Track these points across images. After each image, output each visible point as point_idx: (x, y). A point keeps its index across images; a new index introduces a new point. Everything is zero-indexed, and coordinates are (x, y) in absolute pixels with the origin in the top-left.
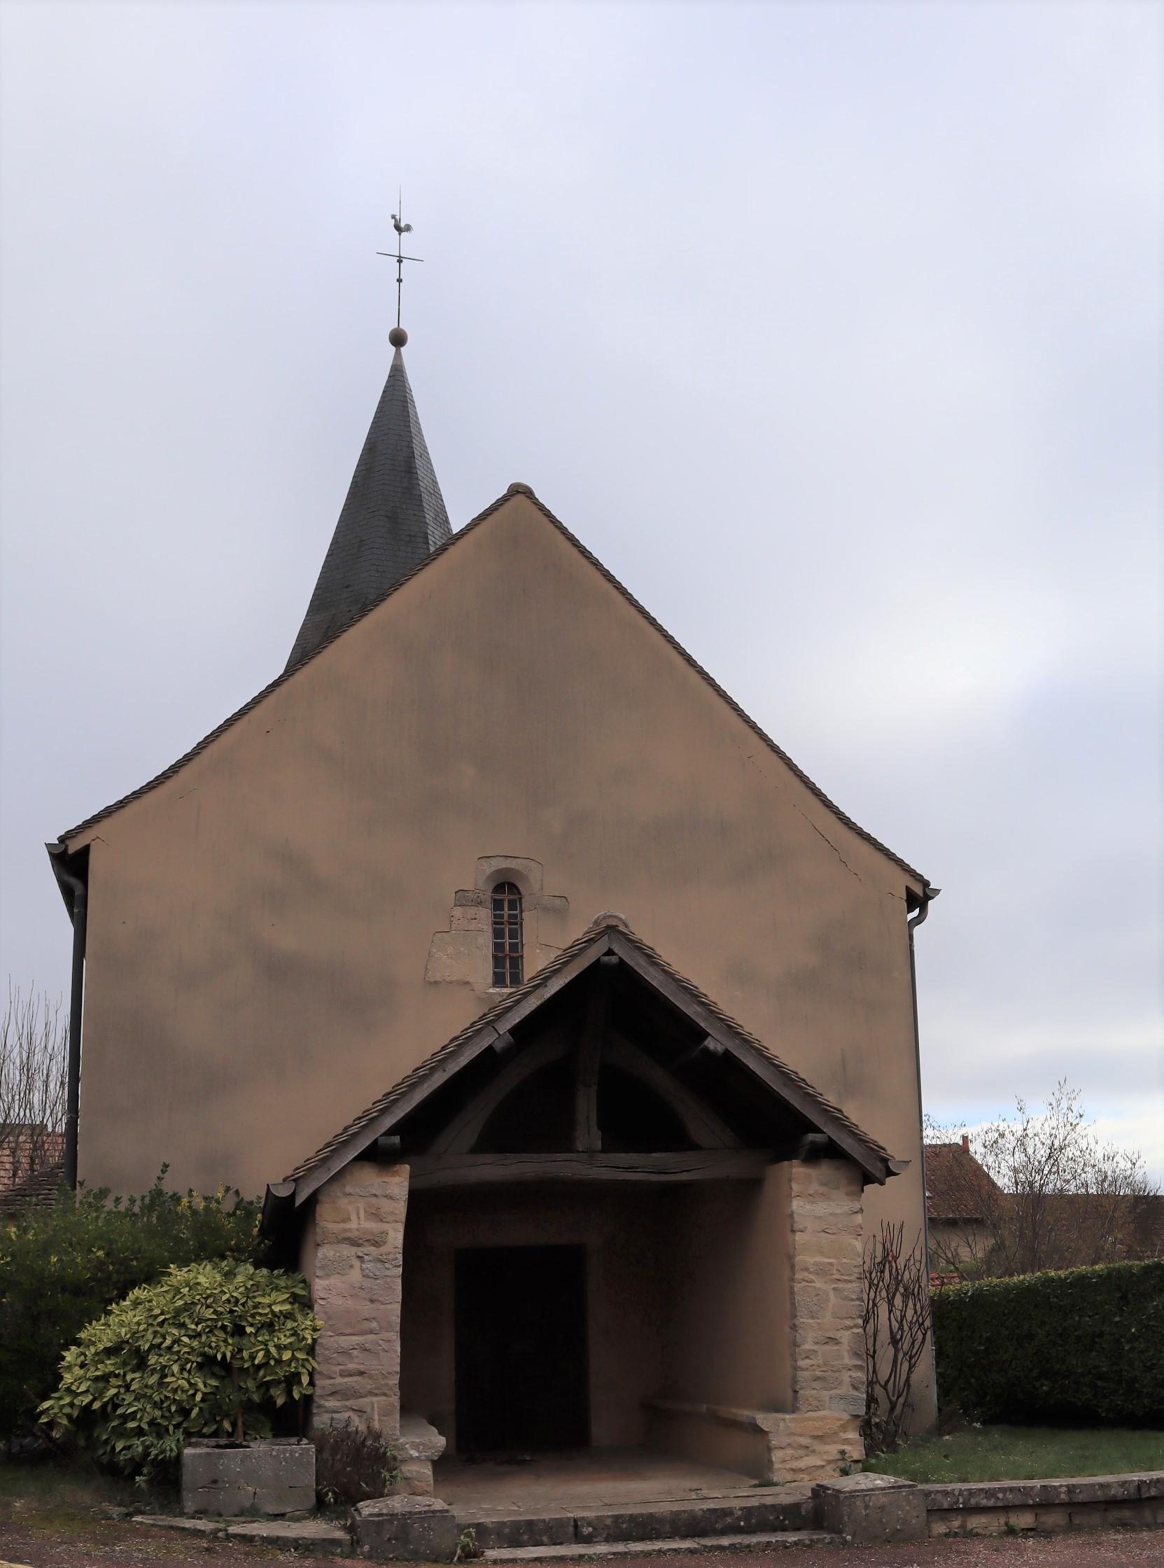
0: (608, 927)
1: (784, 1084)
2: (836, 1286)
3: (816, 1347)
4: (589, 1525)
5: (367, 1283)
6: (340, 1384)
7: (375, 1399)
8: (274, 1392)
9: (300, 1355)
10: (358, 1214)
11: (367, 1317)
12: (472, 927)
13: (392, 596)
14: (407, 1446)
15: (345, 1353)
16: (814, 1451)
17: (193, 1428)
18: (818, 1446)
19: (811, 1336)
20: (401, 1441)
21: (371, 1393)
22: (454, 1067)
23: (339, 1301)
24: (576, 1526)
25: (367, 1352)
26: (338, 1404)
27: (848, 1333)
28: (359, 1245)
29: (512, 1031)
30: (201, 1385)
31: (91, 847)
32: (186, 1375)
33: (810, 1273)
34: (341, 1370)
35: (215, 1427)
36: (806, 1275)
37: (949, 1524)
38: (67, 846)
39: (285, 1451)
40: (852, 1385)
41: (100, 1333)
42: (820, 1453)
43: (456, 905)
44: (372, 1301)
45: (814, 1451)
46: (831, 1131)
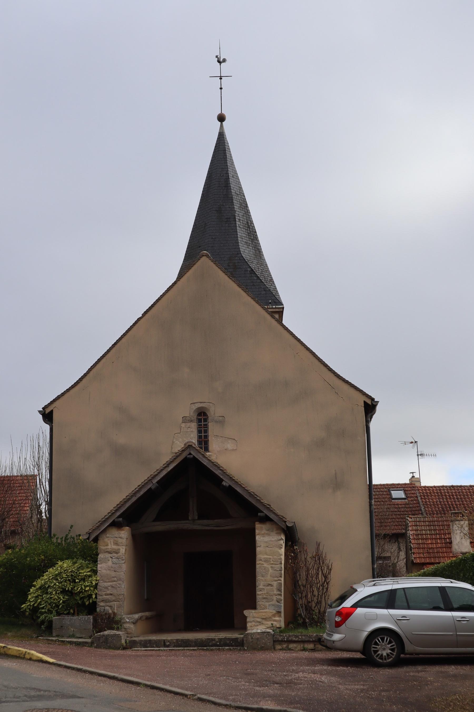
0: (189, 445)
1: (250, 496)
2: (272, 566)
3: (264, 587)
4: (169, 642)
5: (114, 566)
6: (104, 598)
7: (115, 603)
8: (85, 600)
9: (92, 589)
10: (111, 543)
11: (113, 576)
12: (189, 430)
13: (157, 304)
14: (125, 618)
15: (106, 588)
16: (263, 624)
17: (61, 611)
18: (264, 622)
19: (262, 583)
20: (123, 616)
21: (114, 601)
22: (139, 495)
23: (104, 571)
24: (164, 642)
25: (113, 588)
26: (104, 604)
27: (276, 582)
28: (111, 553)
29: (157, 482)
30: (62, 598)
31: (53, 411)
32: (57, 595)
33: (262, 561)
34: (105, 593)
35: (68, 611)
36: (261, 562)
37: (282, 646)
38: (45, 411)
39: (83, 618)
40: (277, 601)
41: (39, 583)
42: (265, 624)
43: (182, 422)
44: (115, 571)
45: (263, 624)
46: (266, 512)
